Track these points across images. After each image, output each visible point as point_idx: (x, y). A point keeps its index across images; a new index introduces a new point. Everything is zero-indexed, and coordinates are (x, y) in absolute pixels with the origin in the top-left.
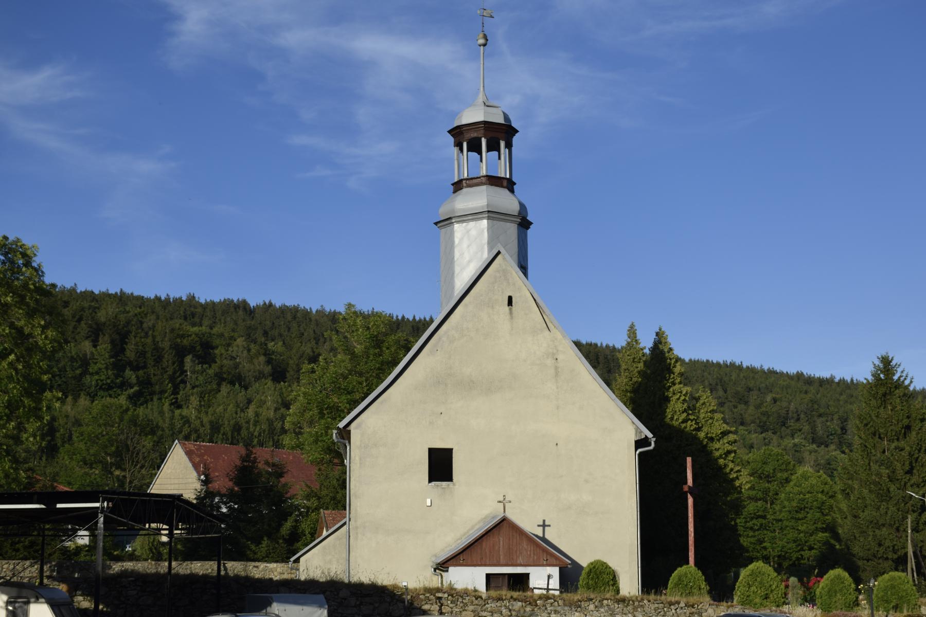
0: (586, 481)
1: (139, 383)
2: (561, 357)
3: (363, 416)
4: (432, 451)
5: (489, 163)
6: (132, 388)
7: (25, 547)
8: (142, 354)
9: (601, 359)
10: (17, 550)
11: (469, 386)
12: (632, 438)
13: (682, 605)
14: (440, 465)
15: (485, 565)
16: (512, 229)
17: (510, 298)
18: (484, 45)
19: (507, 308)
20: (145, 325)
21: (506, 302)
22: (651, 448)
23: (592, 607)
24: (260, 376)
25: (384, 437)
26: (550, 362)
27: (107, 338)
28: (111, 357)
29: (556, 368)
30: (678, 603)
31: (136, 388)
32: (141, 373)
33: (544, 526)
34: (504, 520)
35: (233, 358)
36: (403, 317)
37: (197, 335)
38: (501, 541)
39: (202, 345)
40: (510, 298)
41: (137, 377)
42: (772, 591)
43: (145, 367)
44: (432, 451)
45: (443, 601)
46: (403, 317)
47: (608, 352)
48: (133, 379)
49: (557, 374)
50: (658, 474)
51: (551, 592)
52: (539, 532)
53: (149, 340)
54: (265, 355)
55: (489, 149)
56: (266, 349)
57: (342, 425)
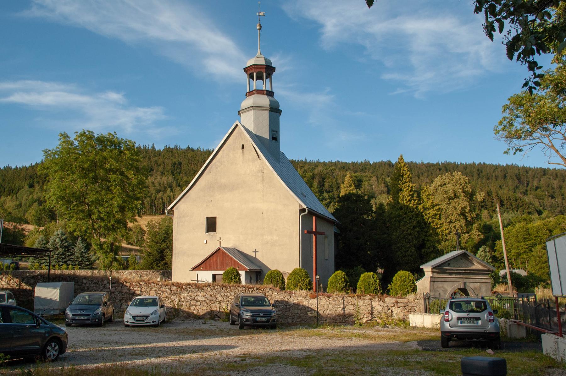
0: (276, 230)
1: (330, 198)
2: (265, 171)
3: (179, 204)
4: (207, 218)
5: (264, 85)
6: (326, 200)
7: (162, 265)
8: (331, 186)
9: (559, 175)
10: (159, 266)
11: (224, 188)
12: (298, 209)
13: (255, 289)
14: (211, 225)
15: (211, 270)
16: (266, 114)
17: (243, 146)
18: (260, 29)
19: (241, 150)
20: (334, 174)
21: (241, 147)
22: (306, 213)
23: (209, 289)
24: (381, 193)
25: (187, 214)
26: (260, 174)
27: (317, 181)
28: (318, 188)
29: (263, 177)
30: (253, 288)
31: (329, 200)
32: (331, 194)
33: (255, 252)
34: (219, 249)
35: (371, 185)
36: (461, 163)
37: (356, 177)
38: (218, 259)
39: (358, 181)
40: (243, 146)
41: (329, 196)
42: (300, 282)
43: (332, 191)
44: (207, 218)
45: (142, 286)
46: (461, 163)
47: (563, 172)
48: (327, 197)
49: (263, 180)
50: (338, 228)
51: (199, 282)
52: (253, 255)
53: (334, 180)
54: (384, 183)
55: (267, 78)
56: (385, 181)
57: (169, 208)
